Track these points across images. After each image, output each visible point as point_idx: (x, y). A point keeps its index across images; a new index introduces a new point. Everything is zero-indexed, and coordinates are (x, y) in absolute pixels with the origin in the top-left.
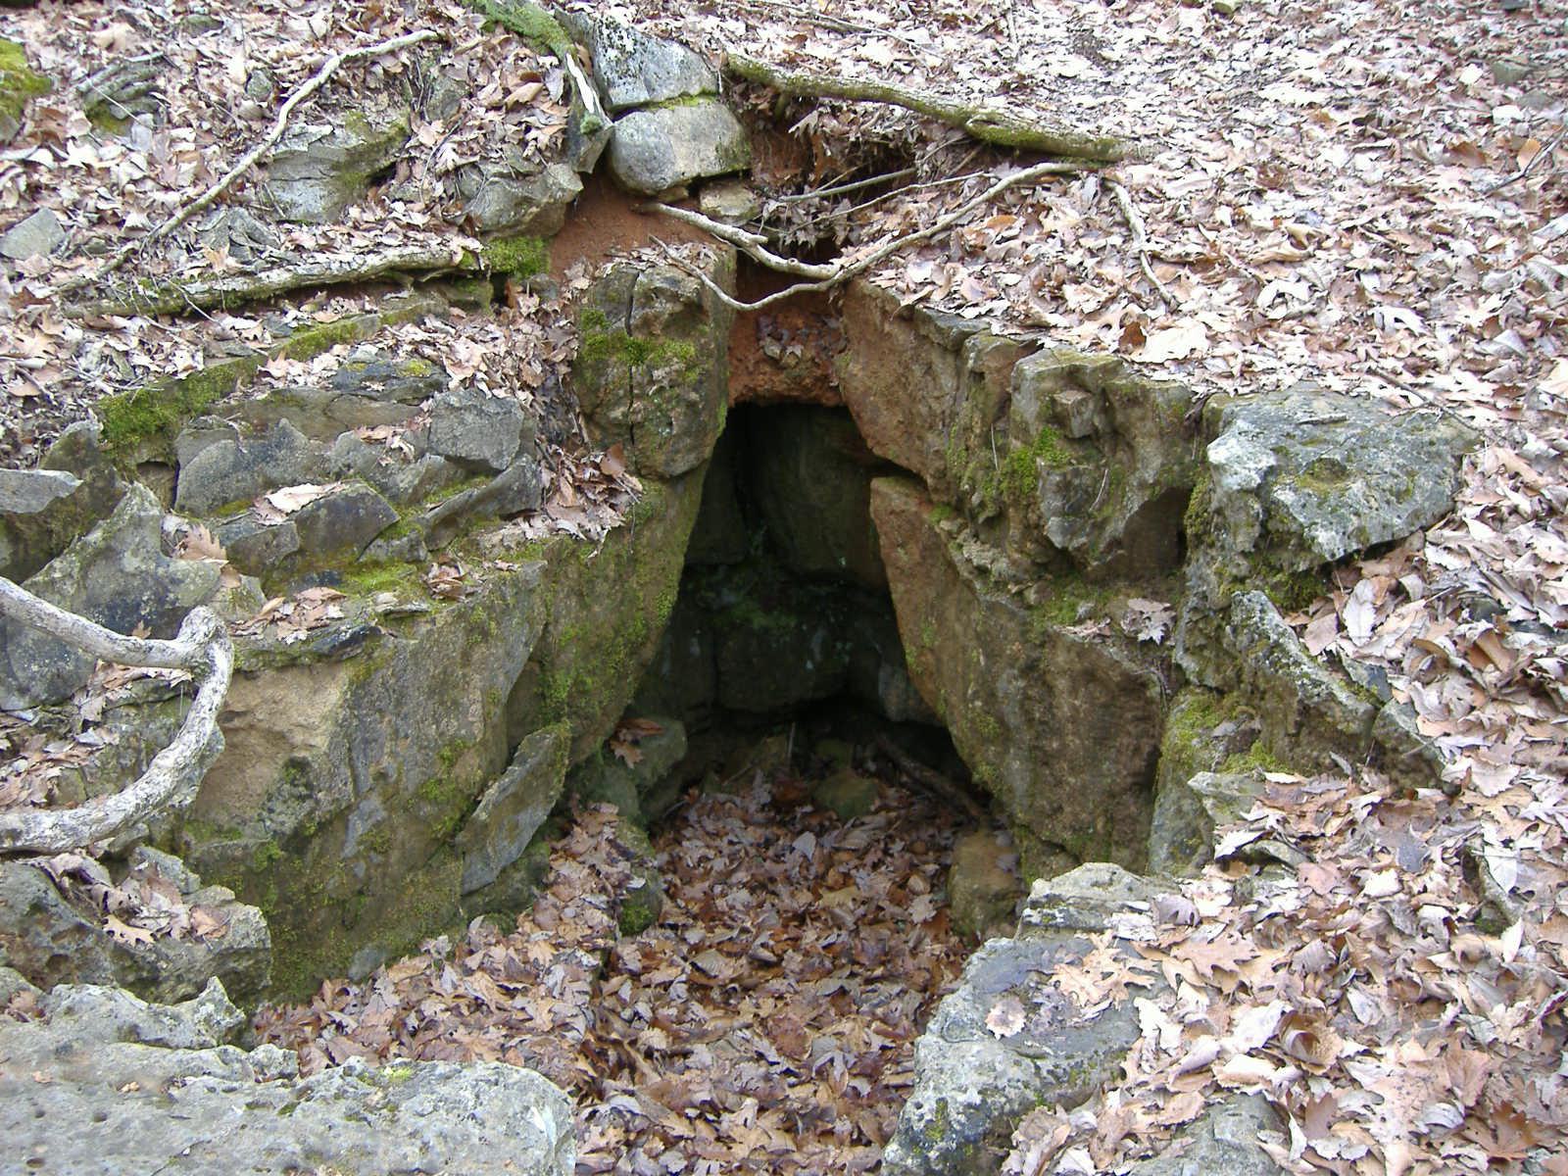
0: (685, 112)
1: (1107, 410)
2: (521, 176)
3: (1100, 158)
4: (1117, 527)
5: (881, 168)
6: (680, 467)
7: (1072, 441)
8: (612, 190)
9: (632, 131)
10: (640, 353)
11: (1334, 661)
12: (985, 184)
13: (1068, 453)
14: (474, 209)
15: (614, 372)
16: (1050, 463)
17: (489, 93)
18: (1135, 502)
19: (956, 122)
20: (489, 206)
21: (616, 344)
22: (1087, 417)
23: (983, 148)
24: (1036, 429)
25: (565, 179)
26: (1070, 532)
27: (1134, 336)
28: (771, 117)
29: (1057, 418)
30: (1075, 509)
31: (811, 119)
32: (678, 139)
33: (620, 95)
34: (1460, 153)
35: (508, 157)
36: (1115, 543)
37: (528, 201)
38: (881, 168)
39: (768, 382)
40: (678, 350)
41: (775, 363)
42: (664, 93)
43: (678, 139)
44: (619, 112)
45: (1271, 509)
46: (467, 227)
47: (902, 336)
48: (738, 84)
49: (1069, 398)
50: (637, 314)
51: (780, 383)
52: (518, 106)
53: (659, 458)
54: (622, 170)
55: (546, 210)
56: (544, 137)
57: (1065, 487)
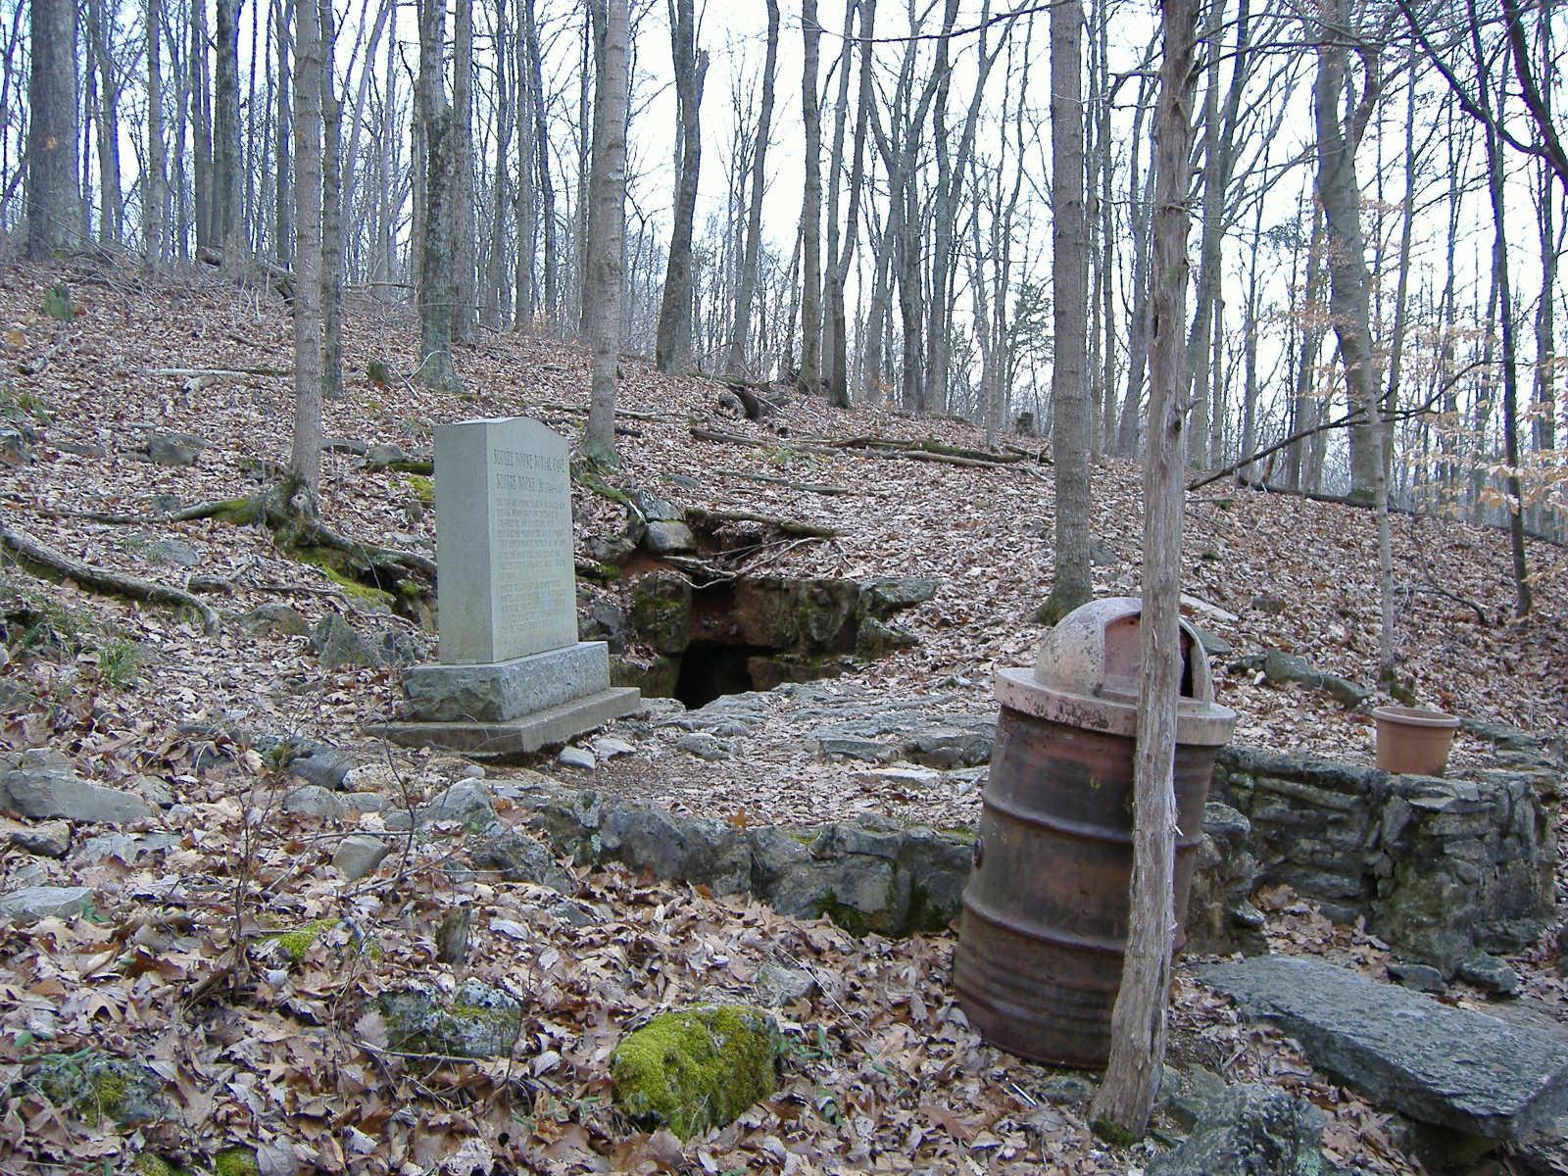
0: (672, 524)
1: (831, 594)
2: (613, 542)
3: (829, 535)
4: (836, 632)
5: (749, 544)
6: (675, 649)
7: (819, 605)
8: (647, 550)
9: (653, 527)
10: (659, 605)
11: (893, 628)
12: (788, 544)
13: (817, 609)
14: (597, 552)
15: (649, 611)
16: (812, 611)
17: (599, 514)
18: (841, 623)
19: (778, 525)
20: (602, 551)
21: (651, 601)
22: (824, 597)
23: (787, 532)
24: (807, 601)
25: (629, 544)
26: (820, 635)
27: (839, 573)
28: (704, 529)
29: (814, 597)
30: (821, 627)
31: (721, 530)
32: (672, 534)
33: (651, 514)
34: (957, 526)
35: (606, 535)
36: (836, 637)
37: (615, 551)
38: (749, 544)
39: (703, 635)
40: (672, 606)
41: (707, 628)
42: (664, 517)
43: (672, 534)
44: (650, 521)
45: (876, 594)
46: (594, 557)
47: (760, 593)
48: (692, 518)
49: (817, 590)
50: (659, 590)
51: (709, 635)
52: (610, 519)
53: (666, 646)
54: (650, 542)
55: (623, 554)
56: (621, 530)
57: (817, 619)
